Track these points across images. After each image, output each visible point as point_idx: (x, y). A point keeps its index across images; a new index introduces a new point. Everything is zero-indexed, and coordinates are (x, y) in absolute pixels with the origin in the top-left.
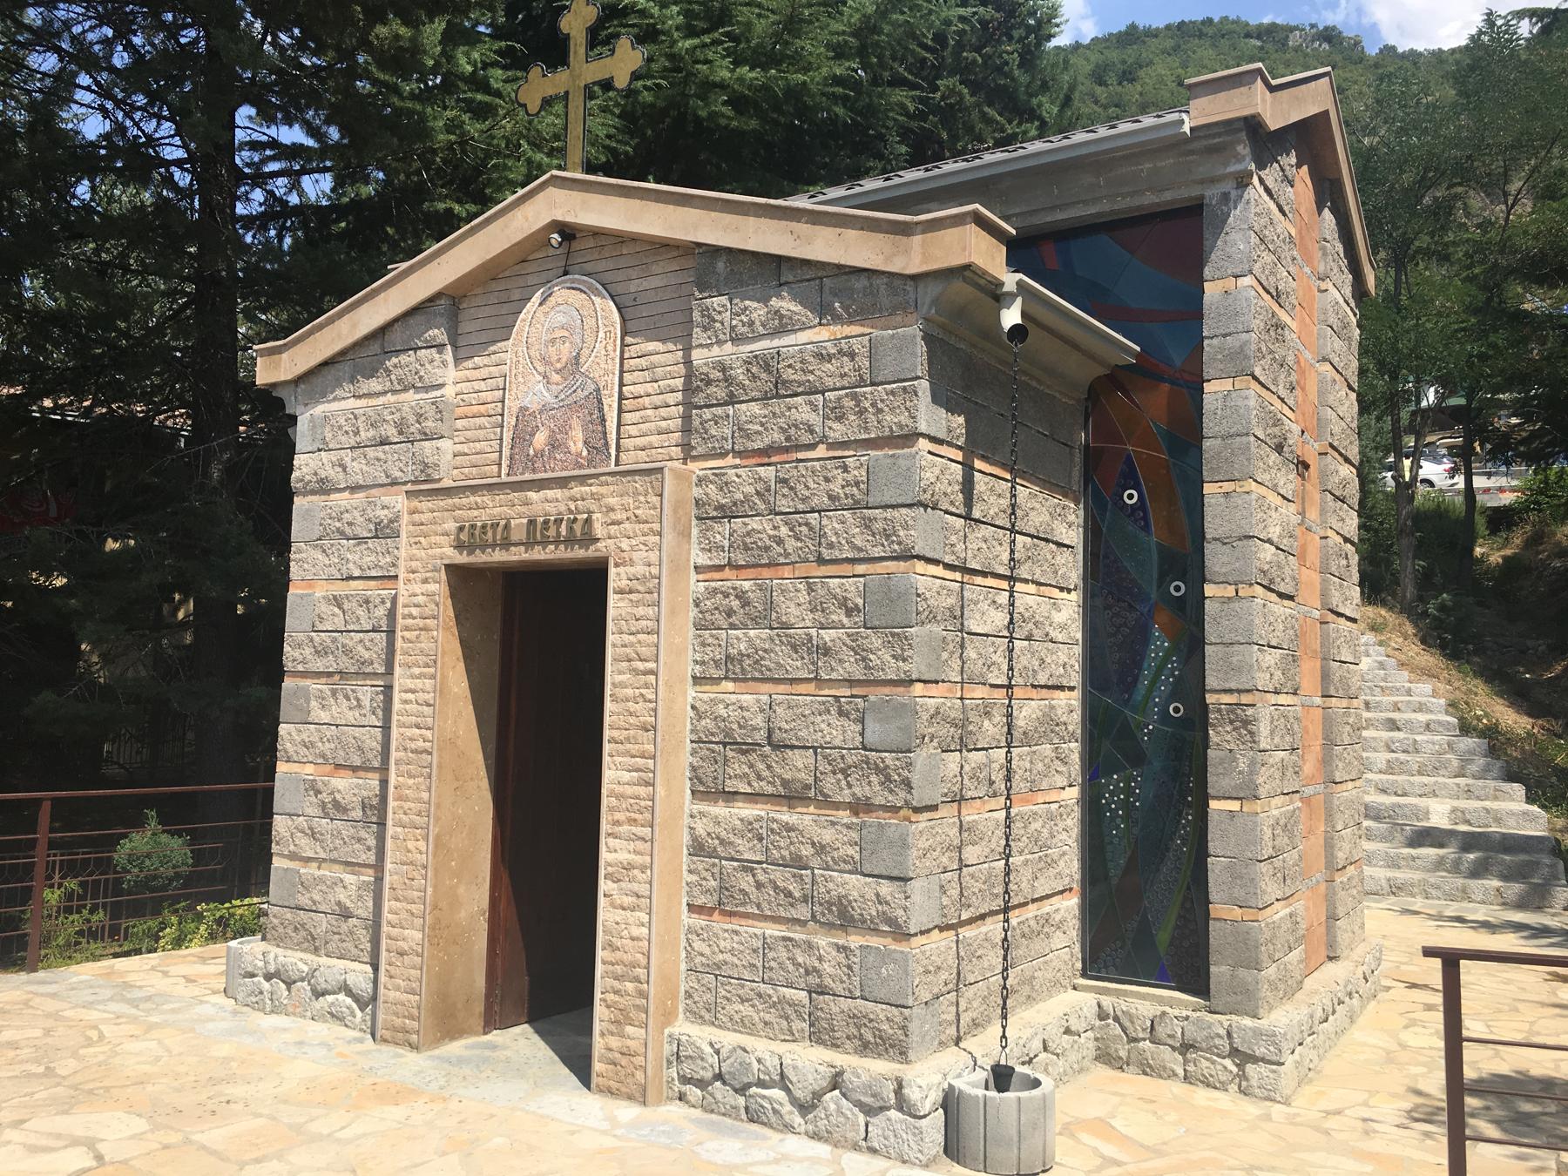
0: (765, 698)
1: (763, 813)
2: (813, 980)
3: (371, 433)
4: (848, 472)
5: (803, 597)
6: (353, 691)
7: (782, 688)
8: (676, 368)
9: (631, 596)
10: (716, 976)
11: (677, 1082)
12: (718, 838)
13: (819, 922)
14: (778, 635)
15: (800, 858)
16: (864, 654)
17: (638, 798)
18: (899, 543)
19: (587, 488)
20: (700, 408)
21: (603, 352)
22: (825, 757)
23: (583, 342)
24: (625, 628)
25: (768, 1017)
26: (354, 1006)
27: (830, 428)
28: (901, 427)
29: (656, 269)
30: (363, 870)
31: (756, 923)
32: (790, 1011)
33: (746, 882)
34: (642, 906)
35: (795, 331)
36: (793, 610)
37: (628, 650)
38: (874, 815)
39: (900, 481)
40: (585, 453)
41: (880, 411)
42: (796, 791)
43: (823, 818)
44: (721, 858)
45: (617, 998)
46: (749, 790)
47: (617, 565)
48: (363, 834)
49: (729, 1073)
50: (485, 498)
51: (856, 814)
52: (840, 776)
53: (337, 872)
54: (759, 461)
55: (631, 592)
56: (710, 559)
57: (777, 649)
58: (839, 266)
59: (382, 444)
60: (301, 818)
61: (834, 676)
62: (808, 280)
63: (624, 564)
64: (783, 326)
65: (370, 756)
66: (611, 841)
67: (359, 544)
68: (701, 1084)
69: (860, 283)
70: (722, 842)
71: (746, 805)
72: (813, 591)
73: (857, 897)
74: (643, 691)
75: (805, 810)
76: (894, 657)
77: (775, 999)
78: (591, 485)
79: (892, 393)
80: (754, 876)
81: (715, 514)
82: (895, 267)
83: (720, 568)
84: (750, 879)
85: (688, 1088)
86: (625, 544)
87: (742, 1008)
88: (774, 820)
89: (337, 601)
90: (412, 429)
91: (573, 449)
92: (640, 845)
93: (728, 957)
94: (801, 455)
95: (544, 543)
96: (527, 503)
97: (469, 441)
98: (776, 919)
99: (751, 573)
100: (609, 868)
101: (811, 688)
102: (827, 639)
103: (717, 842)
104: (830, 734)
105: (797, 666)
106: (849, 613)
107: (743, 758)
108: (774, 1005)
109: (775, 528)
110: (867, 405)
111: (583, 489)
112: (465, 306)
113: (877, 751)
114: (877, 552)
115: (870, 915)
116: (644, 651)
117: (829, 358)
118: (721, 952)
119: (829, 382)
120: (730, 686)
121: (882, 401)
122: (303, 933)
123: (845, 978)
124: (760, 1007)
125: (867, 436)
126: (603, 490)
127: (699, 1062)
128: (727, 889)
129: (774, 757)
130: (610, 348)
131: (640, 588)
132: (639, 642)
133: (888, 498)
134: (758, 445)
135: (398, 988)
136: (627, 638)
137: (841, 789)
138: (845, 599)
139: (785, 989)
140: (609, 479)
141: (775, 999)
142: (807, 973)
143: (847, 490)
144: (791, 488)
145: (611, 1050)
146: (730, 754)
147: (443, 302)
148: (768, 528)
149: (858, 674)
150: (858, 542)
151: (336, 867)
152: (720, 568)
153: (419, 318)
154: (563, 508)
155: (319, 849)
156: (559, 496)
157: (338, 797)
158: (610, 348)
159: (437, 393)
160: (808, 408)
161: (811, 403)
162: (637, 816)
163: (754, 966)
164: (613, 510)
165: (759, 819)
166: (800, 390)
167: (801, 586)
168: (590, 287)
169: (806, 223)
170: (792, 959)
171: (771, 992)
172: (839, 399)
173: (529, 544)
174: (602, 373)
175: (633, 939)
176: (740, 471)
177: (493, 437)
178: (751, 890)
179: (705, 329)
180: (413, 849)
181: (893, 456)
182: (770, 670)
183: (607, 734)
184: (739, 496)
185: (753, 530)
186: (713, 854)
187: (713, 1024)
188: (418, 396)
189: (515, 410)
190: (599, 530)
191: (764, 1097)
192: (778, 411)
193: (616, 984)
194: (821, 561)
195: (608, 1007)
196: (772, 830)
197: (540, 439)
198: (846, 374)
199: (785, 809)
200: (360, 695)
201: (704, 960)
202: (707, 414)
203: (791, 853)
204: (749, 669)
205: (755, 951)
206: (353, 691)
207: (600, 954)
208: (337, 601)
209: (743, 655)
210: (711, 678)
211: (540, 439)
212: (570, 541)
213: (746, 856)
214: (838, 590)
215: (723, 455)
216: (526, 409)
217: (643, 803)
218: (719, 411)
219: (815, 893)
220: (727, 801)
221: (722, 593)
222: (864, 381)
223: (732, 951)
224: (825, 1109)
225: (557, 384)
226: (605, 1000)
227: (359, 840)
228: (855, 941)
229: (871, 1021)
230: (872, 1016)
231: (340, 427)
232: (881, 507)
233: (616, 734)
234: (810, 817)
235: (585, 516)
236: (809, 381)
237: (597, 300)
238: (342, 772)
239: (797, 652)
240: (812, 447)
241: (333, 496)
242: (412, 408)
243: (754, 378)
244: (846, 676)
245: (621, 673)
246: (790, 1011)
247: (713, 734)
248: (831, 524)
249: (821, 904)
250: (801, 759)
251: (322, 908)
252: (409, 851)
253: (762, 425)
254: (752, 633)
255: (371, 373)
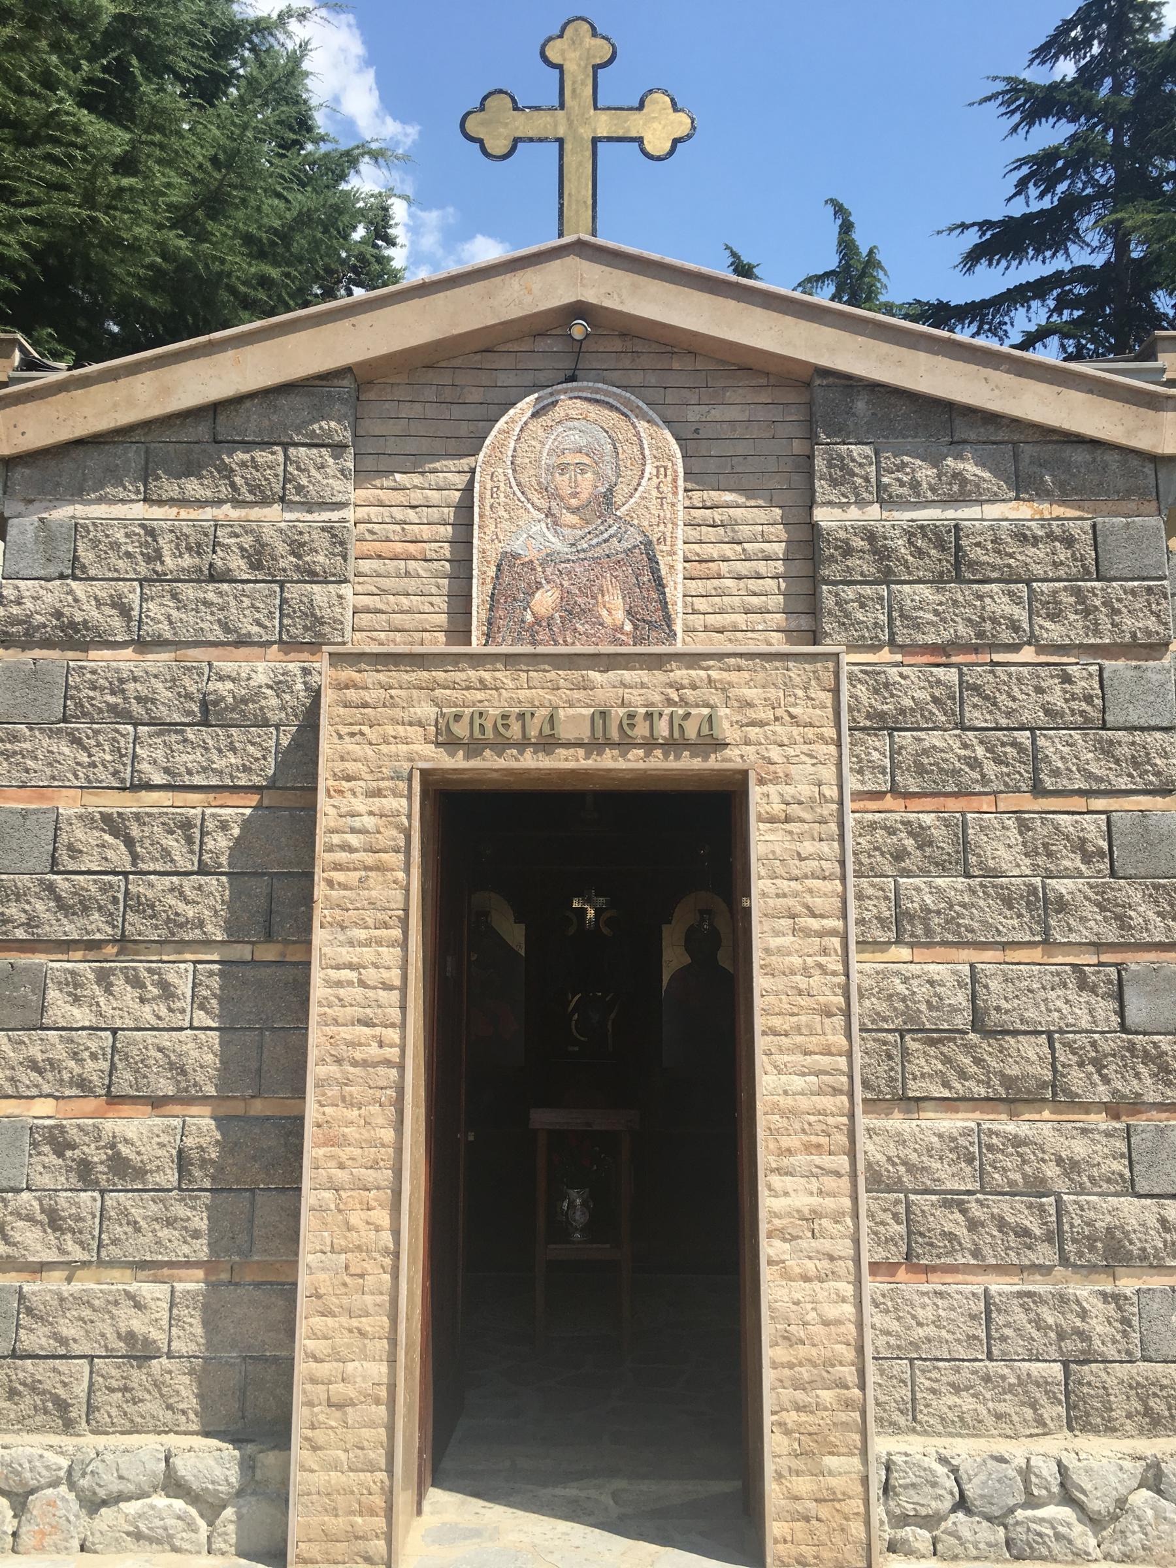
0: (966, 969)
1: (973, 1125)
2: (1072, 1346)
3: (188, 561)
4: (1071, 682)
5: (1014, 835)
6: (149, 970)
7: (989, 955)
8: (772, 529)
9: (788, 826)
10: (911, 1360)
11: (886, 1527)
12: (904, 1163)
13: (1074, 1266)
14: (981, 885)
15: (1043, 1181)
16: (1119, 910)
17: (822, 1113)
18: (1158, 774)
19: (702, 673)
20: (835, 583)
21: (655, 493)
22: (1068, 1045)
23: (619, 476)
24: (780, 871)
25: (1002, 1408)
26: (193, 1512)
27: (1041, 627)
28: (1148, 632)
29: (729, 395)
30: (182, 1273)
31: (970, 1278)
32: (1038, 1394)
33: (954, 1223)
34: (842, 1272)
35: (981, 503)
36: (1002, 852)
37: (790, 902)
38: (1144, 1117)
39: (1152, 698)
40: (628, 627)
41: (1117, 612)
42: (1029, 1092)
43: (1069, 1125)
44: (906, 1192)
45: (804, 1417)
46: (946, 1093)
47: (761, 782)
48: (180, 1210)
49: (982, 1496)
50: (498, 674)
51: (1117, 1117)
52: (1090, 1068)
53: (120, 1282)
54: (933, 660)
55: (787, 820)
56: (863, 782)
57: (982, 903)
58: (1052, 431)
59: (212, 579)
60: (25, 1195)
61: (1074, 938)
62: (994, 443)
63: (775, 780)
64: (965, 493)
65: (200, 1077)
66: (776, 1180)
67: (159, 734)
68: (930, 1521)
69: (1079, 456)
70: (911, 1168)
71: (939, 1115)
72: (1029, 829)
73: (1136, 1227)
74: (822, 960)
75: (1037, 1117)
76: (1159, 914)
77: (1013, 1380)
78: (707, 669)
79: (1133, 592)
80: (964, 1212)
81: (868, 723)
82: (1143, 441)
83: (878, 795)
84: (958, 1216)
85: (908, 1532)
86: (775, 753)
87: (959, 1401)
88: (991, 1132)
89: (113, 824)
90: (283, 563)
91: (608, 620)
92: (830, 1182)
93: (931, 1331)
94: (997, 657)
95: (625, 744)
96: (587, 686)
97: (383, 592)
98: (1001, 1269)
99: (930, 804)
100: (776, 1222)
101: (1036, 954)
102: (1064, 891)
103: (902, 1169)
104: (1072, 1013)
105: (1011, 925)
106: (1087, 858)
107: (932, 1051)
108: (1011, 1389)
109: (965, 746)
110: (1098, 603)
111: (693, 673)
112: (371, 396)
113: (1145, 1033)
114: (1123, 783)
115: (1155, 1248)
116: (818, 903)
117: (1035, 541)
118: (920, 1324)
119: (1038, 570)
120: (904, 953)
121: (1119, 600)
122: (29, 1399)
123: (1118, 1337)
124: (988, 1396)
125: (1099, 641)
126: (733, 677)
127: (928, 1489)
128: (922, 1235)
129: (986, 1048)
130: (667, 489)
131: (806, 816)
132: (810, 891)
133: (1135, 716)
134: (931, 639)
135: (335, 1466)
136: (785, 885)
137: (1093, 1085)
138: (1083, 841)
139: (1027, 1364)
140: (743, 662)
141: (1013, 1380)
142: (1061, 1336)
143: (1075, 705)
144: (987, 698)
145: (797, 1498)
146: (913, 1045)
147: (345, 383)
148: (956, 745)
149: (1111, 934)
150: (1094, 768)
151: (116, 1273)
152: (878, 795)
153: (296, 400)
154: (657, 698)
155: (70, 1245)
156: (645, 680)
157: (125, 1150)
158: (667, 489)
159: (335, 515)
160: (1005, 599)
161: (1011, 594)
162: (823, 1140)
163: (975, 1337)
164: (750, 705)
165: (967, 1133)
166: (995, 575)
167: (1010, 822)
168: (627, 402)
169: (1008, 372)
170: (1038, 1323)
171: (1006, 1371)
172: (1055, 592)
173: (594, 746)
174: (655, 521)
175: (826, 1323)
176: (905, 670)
177: (434, 590)
178: (962, 1232)
179: (834, 483)
180: (361, 1225)
181: (1137, 668)
182: (972, 931)
183: (760, 1022)
184: (908, 703)
185: (934, 747)
186: (895, 1186)
187: (914, 1430)
188: (289, 516)
189: (493, 556)
190: (727, 731)
191: (1042, 1520)
192: (961, 599)
193: (800, 1396)
194: (1038, 790)
195: (787, 1432)
196: (990, 1148)
197: (545, 601)
198: (1062, 563)
199: (1004, 1116)
200: (171, 977)
201: (892, 1340)
202: (849, 593)
203: (1025, 1176)
204: (939, 930)
205: (973, 1317)
206: (149, 970)
207: (769, 1353)
208: (113, 824)
209: (929, 911)
210: (875, 943)
211: (545, 601)
212: (674, 745)
213: (949, 1186)
214: (1071, 829)
215: (875, 648)
216: (516, 556)
217: (831, 1120)
218: (867, 590)
219: (1066, 1227)
220: (908, 1111)
221: (885, 828)
222: (1089, 573)
223: (937, 1322)
224: (1139, 1518)
225: (573, 527)
226: (781, 1424)
227: (170, 1223)
228: (1128, 1284)
229: (1162, 1387)
230: (1165, 1382)
231: (115, 546)
232: (1125, 729)
233: (776, 1022)
234: (1049, 1125)
235: (706, 711)
236: (1009, 566)
237: (642, 425)
238: (126, 1109)
239: (1011, 908)
240: (1015, 648)
241: (93, 654)
242: (281, 531)
243: (920, 553)
244: (1094, 939)
245: (777, 933)
246: (1038, 1394)
247: (885, 1019)
248: (1052, 746)
249: (1074, 1241)
250: (1032, 1049)
251: (77, 1349)
252: (349, 1228)
253: (936, 613)
254: (939, 881)
255: (190, 470)
